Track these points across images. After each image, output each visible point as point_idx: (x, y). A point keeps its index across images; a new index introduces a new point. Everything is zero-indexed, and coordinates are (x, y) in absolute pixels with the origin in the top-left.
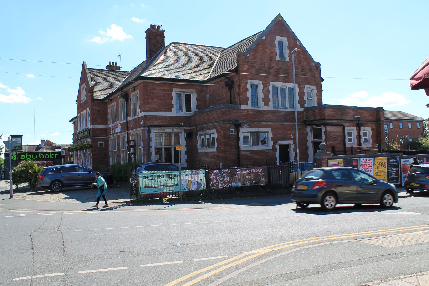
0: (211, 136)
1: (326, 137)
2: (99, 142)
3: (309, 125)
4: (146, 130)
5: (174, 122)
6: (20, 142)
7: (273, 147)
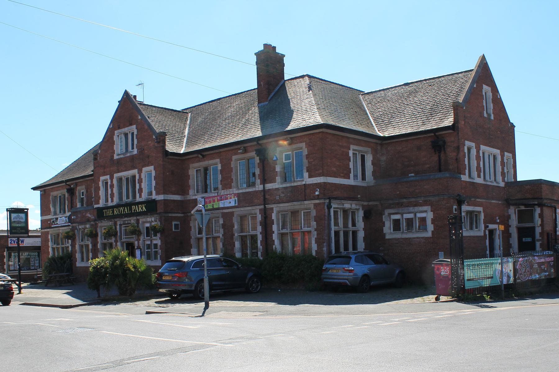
0: (415, 215)
1: (542, 221)
2: (173, 223)
3: (513, 205)
4: (326, 204)
5: (351, 193)
6: (24, 220)
7: (485, 232)
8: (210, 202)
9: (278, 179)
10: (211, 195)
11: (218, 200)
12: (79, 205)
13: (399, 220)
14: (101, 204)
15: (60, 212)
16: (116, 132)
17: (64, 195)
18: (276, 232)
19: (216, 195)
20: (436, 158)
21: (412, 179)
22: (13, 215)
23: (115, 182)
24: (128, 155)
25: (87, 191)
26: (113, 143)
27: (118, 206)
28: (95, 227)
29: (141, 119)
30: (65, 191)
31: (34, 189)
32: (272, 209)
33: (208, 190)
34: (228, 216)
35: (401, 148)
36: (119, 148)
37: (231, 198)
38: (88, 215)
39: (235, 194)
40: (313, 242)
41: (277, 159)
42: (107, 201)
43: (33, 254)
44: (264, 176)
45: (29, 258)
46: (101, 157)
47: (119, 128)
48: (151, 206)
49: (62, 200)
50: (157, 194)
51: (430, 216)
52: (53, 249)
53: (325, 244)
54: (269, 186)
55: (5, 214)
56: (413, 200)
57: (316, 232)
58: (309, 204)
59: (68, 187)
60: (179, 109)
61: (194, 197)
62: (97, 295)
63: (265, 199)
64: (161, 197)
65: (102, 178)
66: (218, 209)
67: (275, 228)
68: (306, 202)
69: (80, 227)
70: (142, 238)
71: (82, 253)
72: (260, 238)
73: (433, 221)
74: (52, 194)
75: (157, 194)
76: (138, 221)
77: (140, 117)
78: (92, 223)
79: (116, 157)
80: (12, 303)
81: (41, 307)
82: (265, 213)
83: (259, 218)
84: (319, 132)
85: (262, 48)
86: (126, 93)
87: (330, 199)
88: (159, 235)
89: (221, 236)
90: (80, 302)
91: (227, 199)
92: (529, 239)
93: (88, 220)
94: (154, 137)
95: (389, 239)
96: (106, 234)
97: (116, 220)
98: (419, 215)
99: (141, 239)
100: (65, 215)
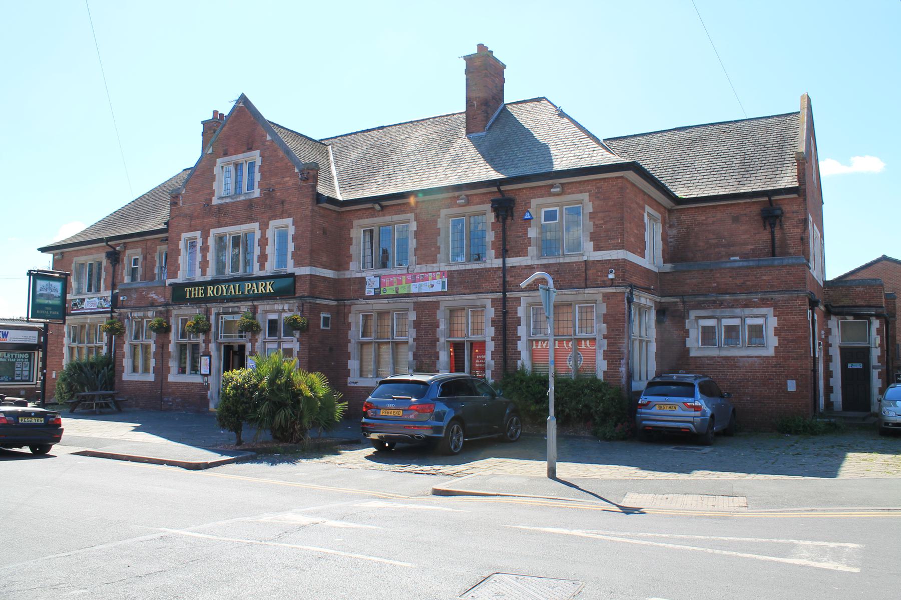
2: (322, 315)
3: (836, 314)
6: (58, 293)
8: (391, 284)
9: (532, 250)
10: (394, 273)
11: (408, 282)
12: (127, 279)
13: (761, 326)
14: (180, 279)
15: (90, 290)
16: (218, 161)
17: (100, 264)
18: (172, 342)
19: (405, 272)
20: (765, 235)
21: (737, 264)
22: (41, 283)
23: (211, 242)
24: (242, 198)
25: (145, 258)
26: (213, 178)
27: (214, 282)
28: (167, 315)
29: (272, 141)
30: (102, 257)
31: (43, 250)
32: (519, 299)
33: (389, 264)
34: (426, 309)
35: (704, 218)
36: (223, 187)
37: (434, 279)
38: (153, 295)
39: (443, 273)
40: (600, 356)
41: (532, 218)
42: (191, 270)
43: (20, 356)
44: (504, 245)
45: (14, 363)
46: (188, 199)
47: (226, 154)
48: (285, 287)
49: (95, 271)
50: (297, 264)
51: (773, 322)
52: (71, 349)
53: (623, 362)
54: (512, 261)
55: (24, 283)
56: (743, 297)
57: (605, 341)
58: (595, 293)
59: (111, 250)
60: (317, 138)
61: (359, 275)
62: (234, 442)
63: (505, 282)
64: (305, 271)
65: (185, 236)
66: (408, 295)
67: (522, 331)
68: (587, 291)
69: (135, 315)
70: (260, 338)
71: (134, 356)
72: (490, 346)
73: (777, 332)
74: (75, 259)
75: (297, 264)
76: (254, 310)
77: (268, 138)
78: (160, 308)
79: (215, 201)
80: (55, 449)
81: (129, 463)
82: (504, 306)
83: (491, 313)
84: (617, 178)
85: (476, 52)
86: (243, 99)
87: (631, 286)
88: (297, 334)
89: (411, 341)
90: (216, 457)
91: (427, 279)
92: (858, 366)
93: (153, 304)
94: (296, 170)
95: (696, 358)
96: (193, 327)
97: (209, 305)
98: (749, 321)
99: (260, 340)
100: (99, 295)
